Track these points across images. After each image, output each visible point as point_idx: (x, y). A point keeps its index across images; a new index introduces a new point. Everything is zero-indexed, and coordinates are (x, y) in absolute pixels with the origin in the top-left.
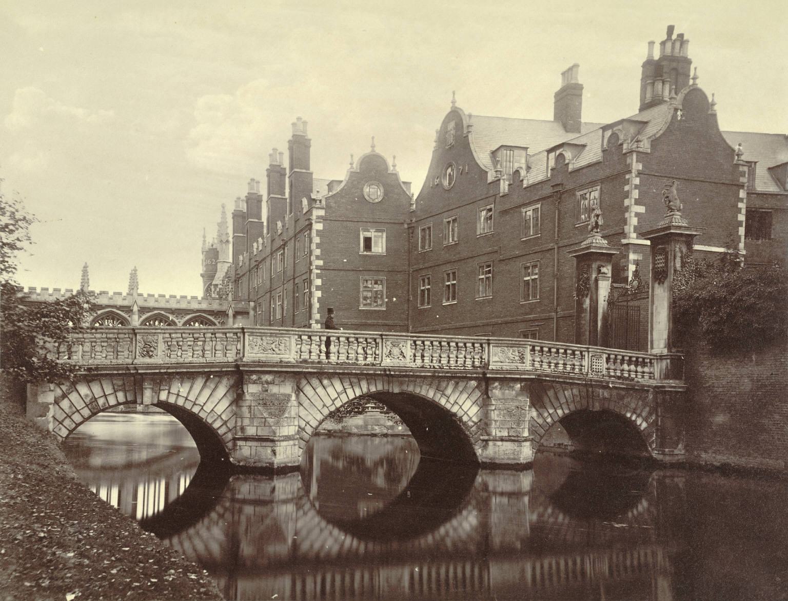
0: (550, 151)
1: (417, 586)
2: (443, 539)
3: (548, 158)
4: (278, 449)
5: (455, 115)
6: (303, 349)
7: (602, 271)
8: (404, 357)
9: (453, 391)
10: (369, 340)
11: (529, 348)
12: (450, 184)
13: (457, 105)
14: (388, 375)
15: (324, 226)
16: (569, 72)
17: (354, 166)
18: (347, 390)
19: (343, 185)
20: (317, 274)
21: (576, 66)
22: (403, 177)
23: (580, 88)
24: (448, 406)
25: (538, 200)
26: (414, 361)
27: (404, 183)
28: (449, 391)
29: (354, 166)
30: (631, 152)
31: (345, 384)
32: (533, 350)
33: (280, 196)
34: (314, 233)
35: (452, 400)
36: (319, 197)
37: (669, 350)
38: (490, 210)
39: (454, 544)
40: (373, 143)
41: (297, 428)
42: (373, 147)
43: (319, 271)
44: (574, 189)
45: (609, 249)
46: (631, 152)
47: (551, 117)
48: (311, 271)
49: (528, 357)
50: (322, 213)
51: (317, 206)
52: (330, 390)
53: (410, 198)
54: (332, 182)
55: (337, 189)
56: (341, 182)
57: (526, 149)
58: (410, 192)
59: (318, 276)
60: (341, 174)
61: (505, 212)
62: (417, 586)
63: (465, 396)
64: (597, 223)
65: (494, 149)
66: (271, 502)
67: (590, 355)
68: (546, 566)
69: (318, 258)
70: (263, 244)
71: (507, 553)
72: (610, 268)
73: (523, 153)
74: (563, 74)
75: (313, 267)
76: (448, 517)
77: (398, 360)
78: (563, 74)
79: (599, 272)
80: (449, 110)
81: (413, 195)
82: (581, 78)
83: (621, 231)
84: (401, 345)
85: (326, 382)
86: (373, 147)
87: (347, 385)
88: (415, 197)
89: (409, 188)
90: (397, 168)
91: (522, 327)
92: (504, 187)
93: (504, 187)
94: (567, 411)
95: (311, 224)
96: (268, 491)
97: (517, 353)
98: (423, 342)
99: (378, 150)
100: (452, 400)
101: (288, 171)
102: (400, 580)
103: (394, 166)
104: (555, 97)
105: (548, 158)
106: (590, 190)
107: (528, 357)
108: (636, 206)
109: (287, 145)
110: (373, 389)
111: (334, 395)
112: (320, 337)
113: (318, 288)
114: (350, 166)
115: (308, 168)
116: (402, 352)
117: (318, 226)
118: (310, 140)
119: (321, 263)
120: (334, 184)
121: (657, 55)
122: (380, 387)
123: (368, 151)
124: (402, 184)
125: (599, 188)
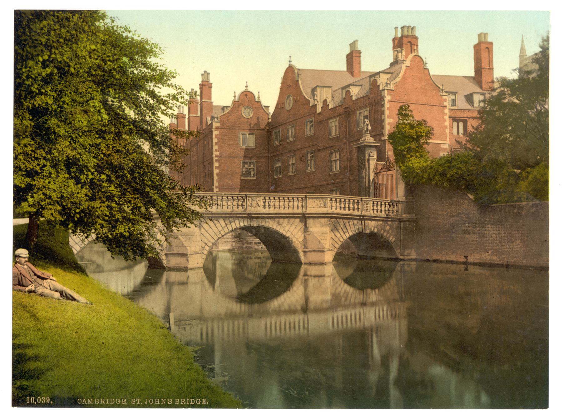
0: (343, 89)
1: (269, 329)
2: (282, 304)
4: (189, 259)
5: (290, 69)
8: (259, 206)
11: (329, 199)
13: (292, 63)
14: (250, 217)
15: (220, 132)
16: (353, 45)
17: (237, 98)
18: (228, 226)
19: (229, 109)
20: (216, 160)
21: (357, 41)
24: (284, 233)
25: (337, 116)
27: (265, 106)
28: (284, 225)
29: (237, 98)
31: (226, 222)
32: (331, 199)
33: (195, 115)
34: (214, 136)
38: (312, 122)
39: (289, 306)
40: (247, 85)
41: (200, 247)
42: (247, 87)
43: (217, 158)
44: (356, 110)
45: (374, 143)
46: (384, 90)
47: (345, 69)
50: (218, 125)
53: (268, 115)
54: (224, 107)
57: (331, 87)
58: (268, 111)
60: (228, 102)
61: (319, 123)
62: (269, 329)
63: (293, 227)
64: (367, 129)
68: (273, 322)
69: (216, 150)
70: (186, 143)
71: (319, 310)
72: (375, 153)
73: (330, 90)
74: (350, 45)
76: (278, 294)
77: (255, 209)
78: (350, 45)
79: (369, 156)
80: (287, 66)
81: (270, 113)
82: (360, 47)
84: (257, 200)
86: (247, 87)
87: (227, 222)
89: (268, 110)
90: (260, 98)
92: (319, 110)
93: (319, 110)
94: (351, 234)
95: (212, 132)
97: (322, 203)
98: (269, 198)
99: (250, 89)
100: (287, 229)
102: (327, 322)
103: (259, 97)
108: (389, 119)
109: (199, 87)
111: (220, 229)
112: (217, 197)
113: (217, 168)
114: (233, 98)
117: (215, 133)
119: (218, 153)
120: (225, 108)
121: (399, 35)
122: (246, 224)
123: (244, 89)
125: (368, 109)
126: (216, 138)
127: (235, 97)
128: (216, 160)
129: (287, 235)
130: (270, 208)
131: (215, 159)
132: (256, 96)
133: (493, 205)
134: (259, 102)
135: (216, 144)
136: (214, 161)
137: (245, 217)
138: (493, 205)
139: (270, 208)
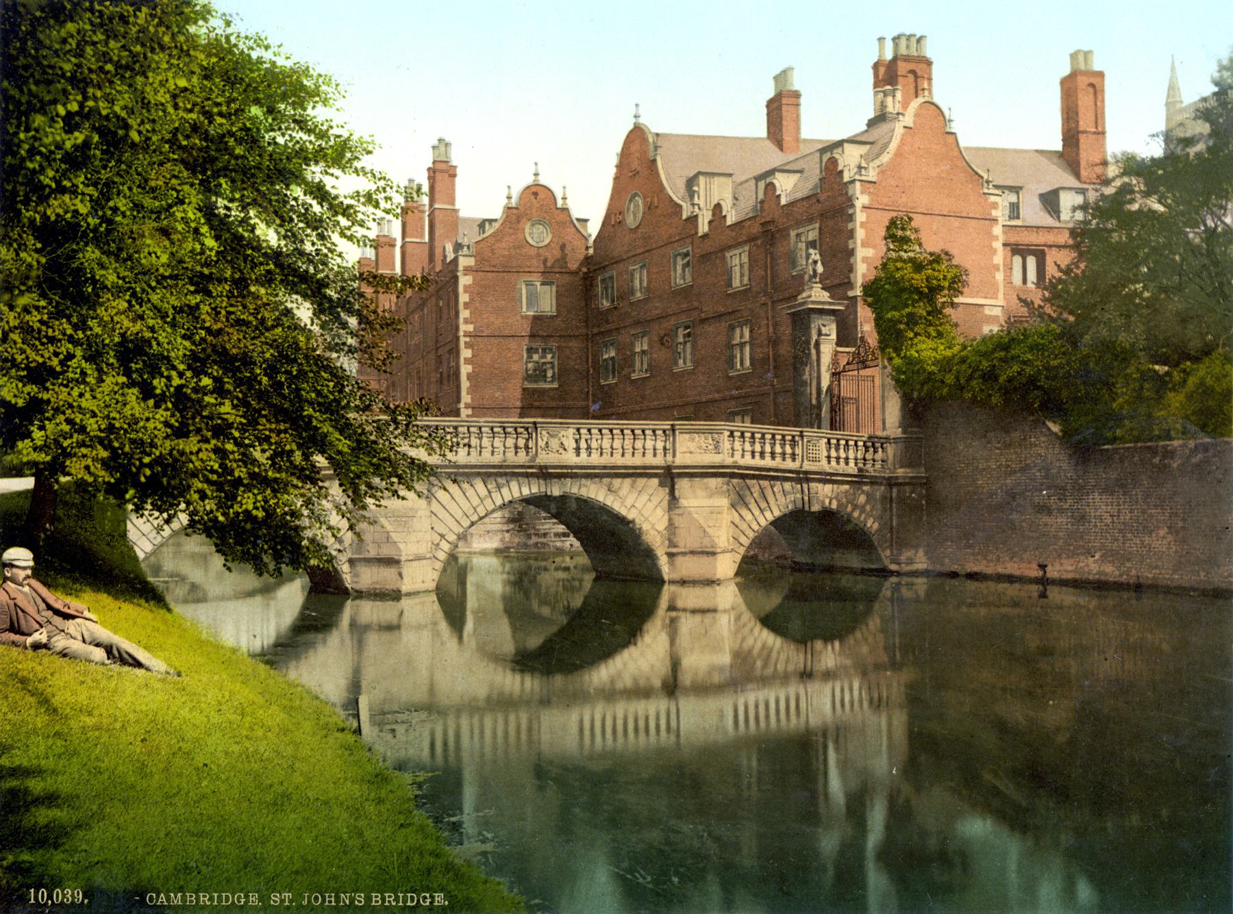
0: (758, 179)
1: (587, 733)
2: (619, 675)
3: (757, 187)
5: (637, 134)
6: (658, 447)
7: (824, 332)
8: (565, 449)
9: (630, 492)
10: (520, 430)
11: (728, 433)
12: (635, 220)
13: (641, 120)
14: (544, 473)
15: (474, 280)
16: (782, 77)
18: (493, 494)
19: (496, 226)
20: (466, 343)
21: (791, 69)
22: (576, 213)
23: (797, 95)
24: (624, 512)
26: (612, 455)
27: (578, 220)
30: (853, 182)
31: (489, 487)
32: (732, 434)
34: (461, 289)
35: (629, 502)
36: (466, 241)
37: (904, 432)
38: (687, 255)
42: (536, 175)
43: (467, 339)
45: (830, 304)
46: (853, 182)
48: (458, 338)
49: (726, 445)
50: (471, 262)
51: (464, 253)
52: (470, 492)
54: (484, 221)
55: (489, 230)
56: (496, 220)
57: (730, 175)
58: (586, 231)
59: (468, 345)
62: (587, 733)
63: (645, 497)
64: (815, 271)
65: (692, 175)
66: (398, 627)
67: (805, 440)
69: (466, 321)
71: (703, 689)
72: (834, 326)
75: (461, 333)
77: (557, 455)
80: (631, 127)
81: (590, 235)
82: (797, 83)
83: (846, 281)
84: (560, 435)
85: (465, 486)
87: (491, 486)
88: (593, 237)
89: (585, 228)
91: (732, 406)
92: (703, 227)
93: (703, 227)
95: (456, 278)
96: (395, 614)
97: (711, 441)
99: (543, 181)
100: (629, 502)
101: (427, 208)
103: (564, 198)
104: (768, 106)
105: (757, 187)
106: (807, 228)
107: (726, 445)
108: (864, 250)
110: (526, 492)
113: (467, 361)
114: (506, 201)
115: (452, 202)
116: (562, 444)
117: (464, 280)
118: (455, 167)
119: (470, 328)
122: (535, 490)
123: (529, 180)
124: (575, 222)
125: (817, 225)
126: (465, 291)
127: (509, 198)
128: (466, 343)
129: (630, 517)
130: (589, 455)
131: (463, 340)
132: (559, 196)
133: (1106, 447)
134: (565, 210)
135: (466, 305)
136: (462, 345)
137: (532, 475)
138: (1106, 447)
139: (589, 455)
